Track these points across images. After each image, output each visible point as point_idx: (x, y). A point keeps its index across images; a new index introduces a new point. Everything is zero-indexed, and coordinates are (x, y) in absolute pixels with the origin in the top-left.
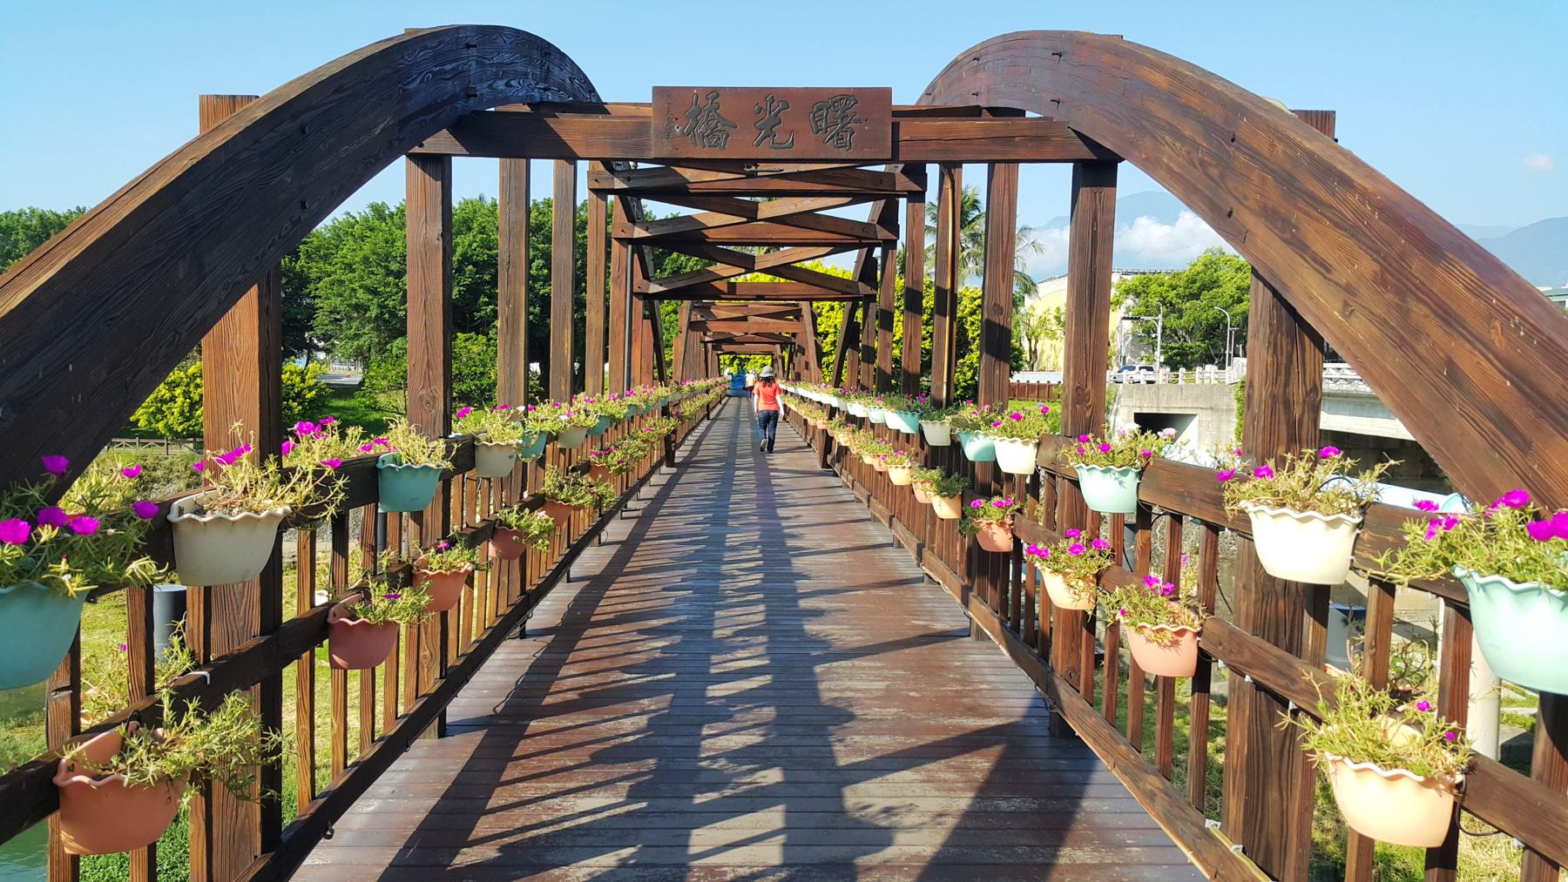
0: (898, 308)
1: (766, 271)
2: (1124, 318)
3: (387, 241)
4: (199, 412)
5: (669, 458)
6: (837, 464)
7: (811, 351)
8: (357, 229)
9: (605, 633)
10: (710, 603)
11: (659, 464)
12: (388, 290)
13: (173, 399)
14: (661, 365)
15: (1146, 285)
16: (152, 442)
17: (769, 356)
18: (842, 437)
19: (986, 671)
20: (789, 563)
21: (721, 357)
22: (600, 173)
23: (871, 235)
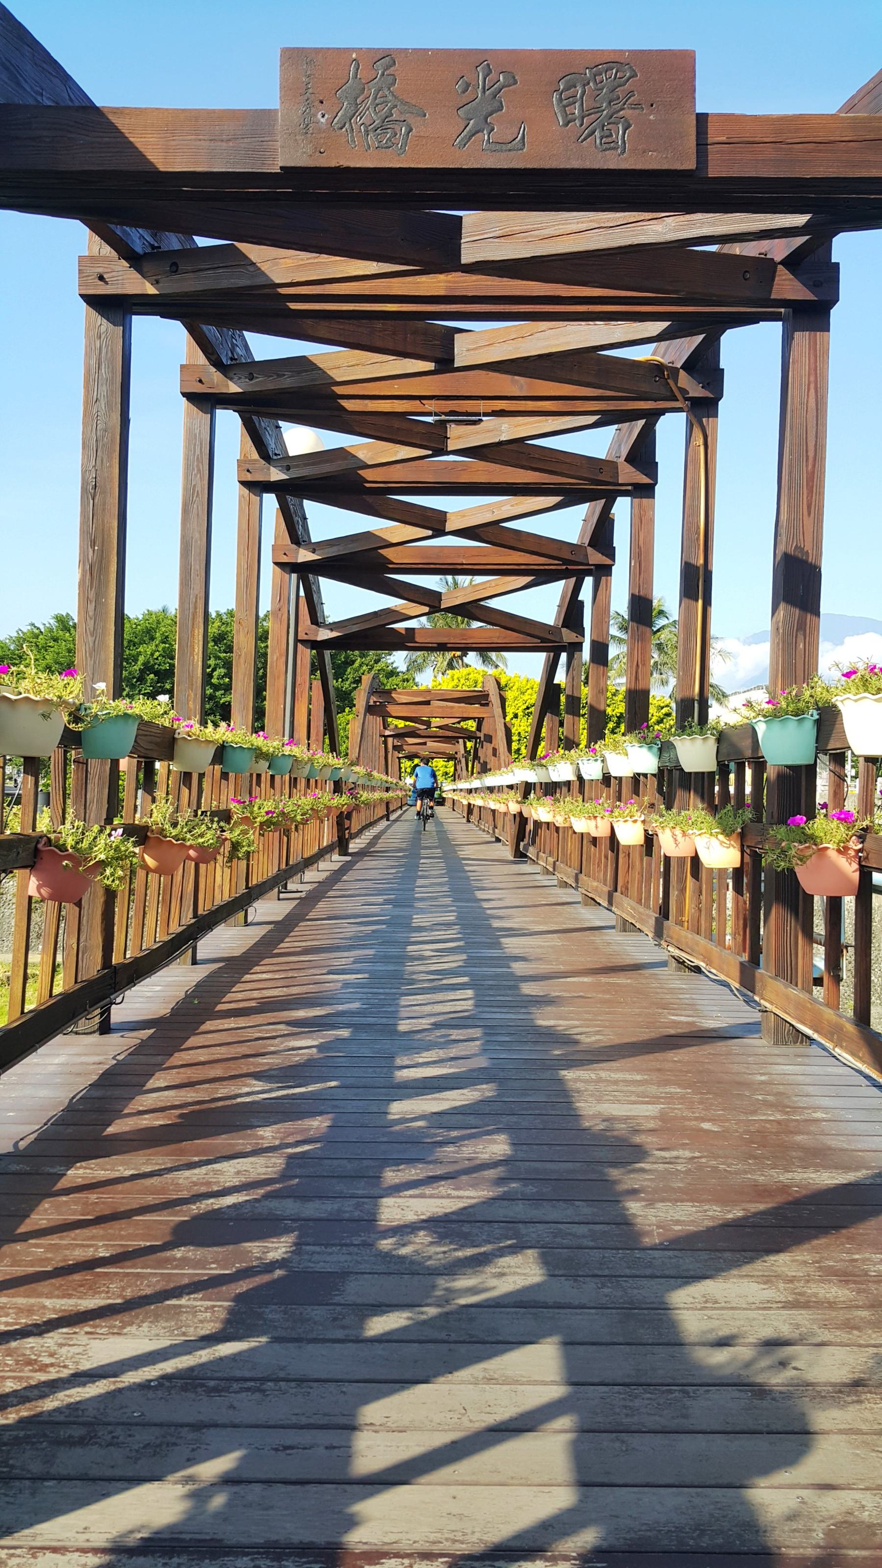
0: (583, 715)
5: (341, 845)
7: (501, 735)
8: (41, 640)
9: (226, 1026)
10: (381, 991)
19: (810, 1090)
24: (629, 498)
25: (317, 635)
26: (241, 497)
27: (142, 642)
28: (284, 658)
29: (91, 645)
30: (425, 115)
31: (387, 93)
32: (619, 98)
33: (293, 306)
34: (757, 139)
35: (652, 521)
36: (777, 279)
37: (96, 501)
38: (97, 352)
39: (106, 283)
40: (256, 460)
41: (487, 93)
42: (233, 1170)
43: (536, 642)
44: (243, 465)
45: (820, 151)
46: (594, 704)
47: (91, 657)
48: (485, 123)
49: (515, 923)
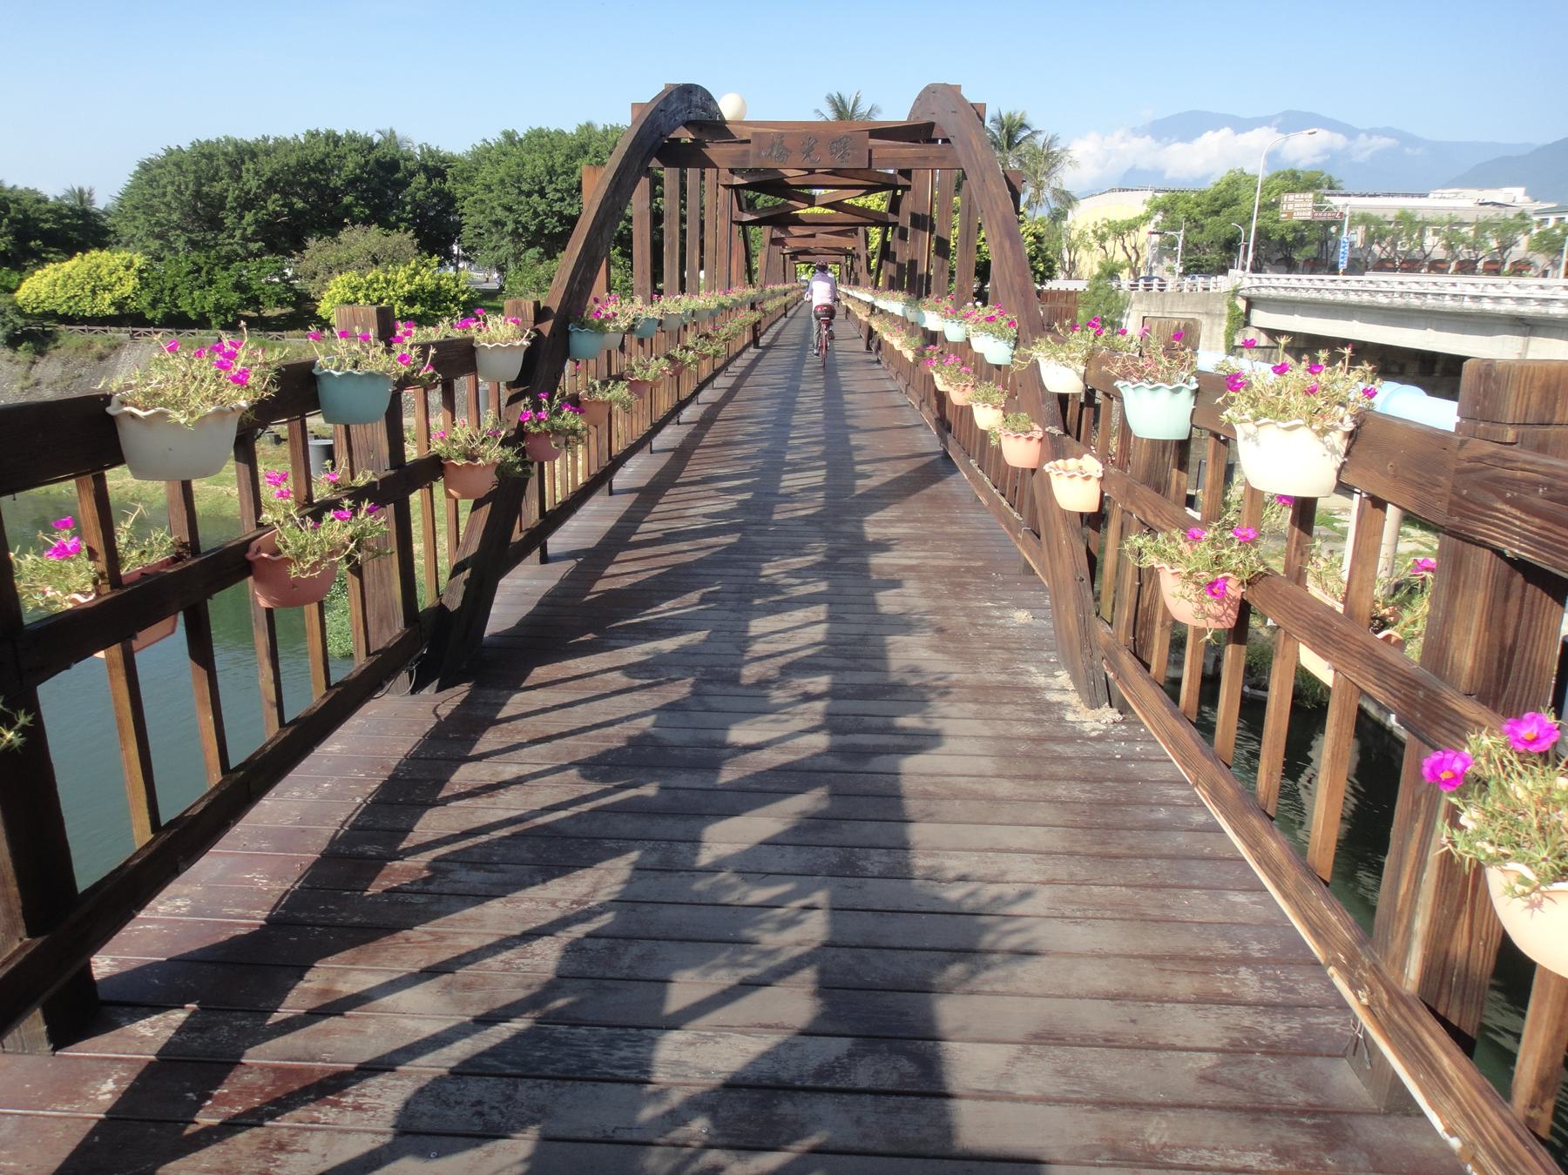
1: (825, 206)
5: (755, 341)
14: (750, 272)
15: (1173, 203)
27: (578, 156)
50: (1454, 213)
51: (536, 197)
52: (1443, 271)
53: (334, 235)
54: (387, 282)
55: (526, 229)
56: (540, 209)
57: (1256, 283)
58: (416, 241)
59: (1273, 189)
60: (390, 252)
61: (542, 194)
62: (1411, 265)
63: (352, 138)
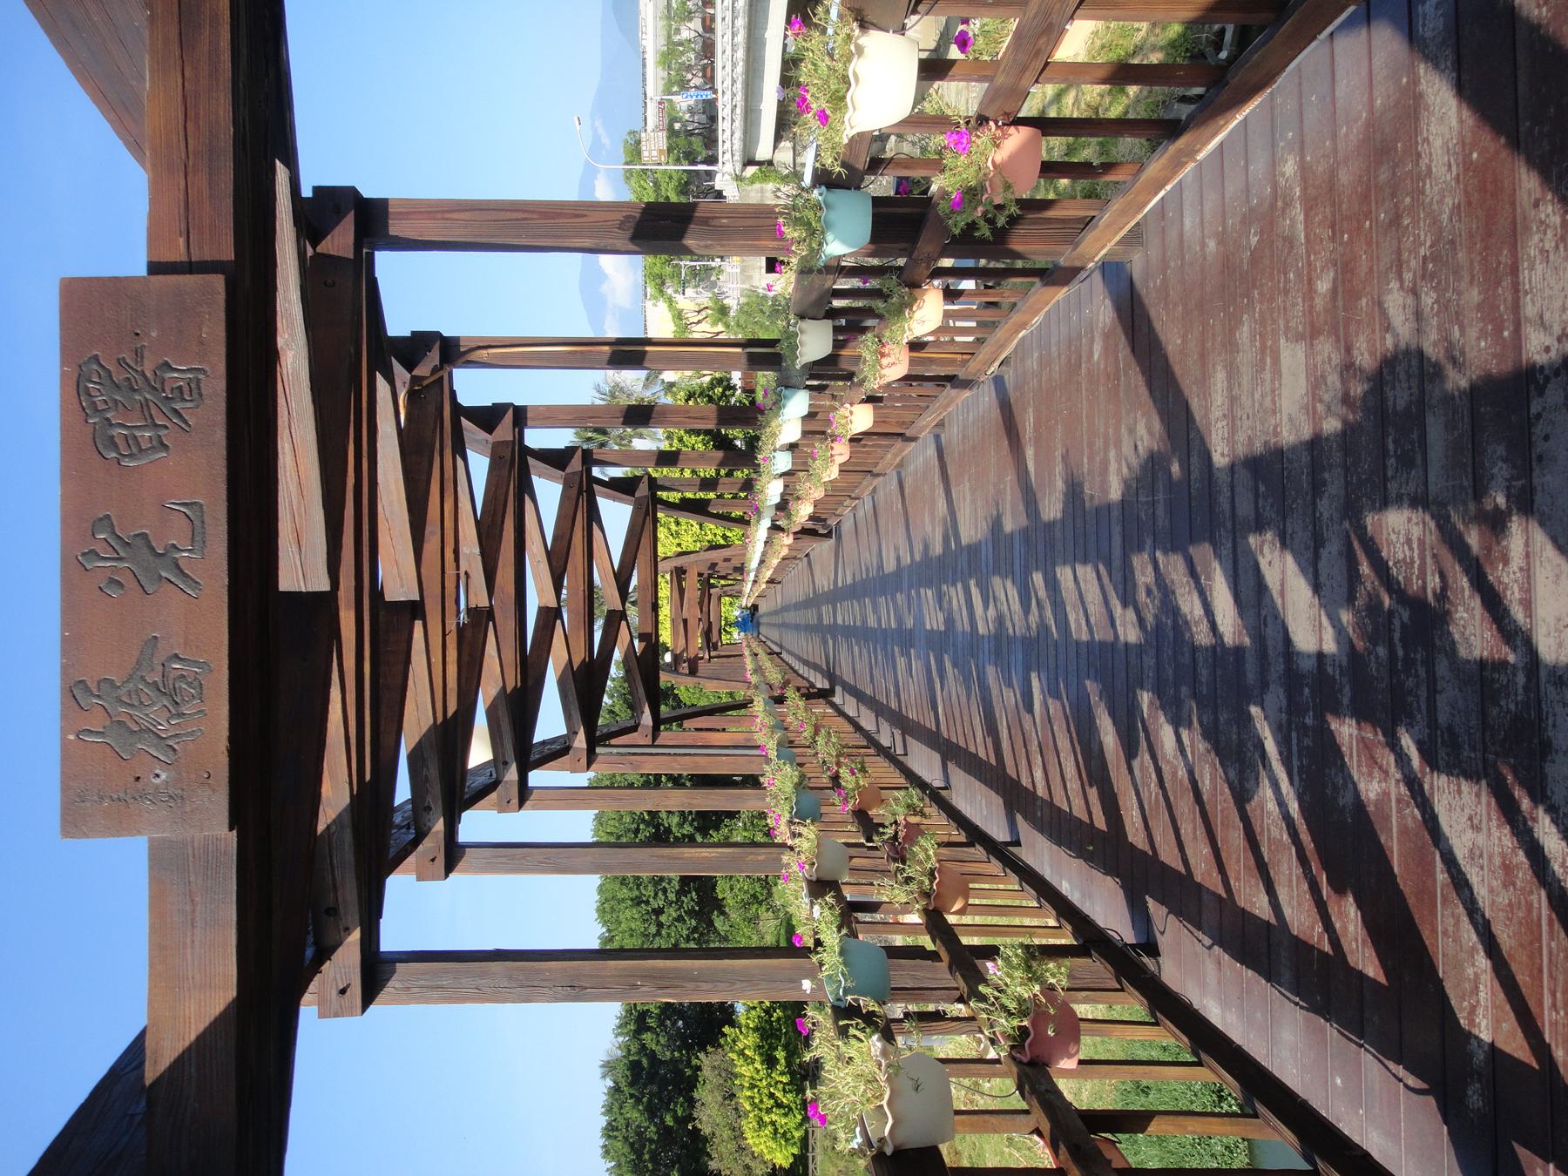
2: (684, 294)
3: (632, 936)
4: (784, 1100)
5: (825, 695)
6: (829, 522)
11: (833, 705)
12: (673, 934)
13: (773, 1123)
16: (811, 1141)
17: (723, 600)
18: (803, 512)
20: (1050, 525)
21: (724, 642)
22: (500, 798)
23: (577, 479)
24: (526, 430)
25: (647, 726)
26: (534, 808)
28: (678, 758)
29: (745, 984)
30: (155, 638)
31: (125, 690)
32: (128, 379)
33: (368, 777)
34: (182, 197)
35: (549, 408)
36: (332, 253)
37: (588, 985)
38: (425, 990)
39: (348, 985)
40: (498, 795)
41: (122, 554)
42: (1470, 834)
43: (649, 520)
44: (503, 807)
45: (197, 114)
46: (718, 462)
47: (758, 984)
48: (166, 556)
49: (934, 530)
50: (659, 15)
51: (663, 918)
52: (713, 18)
53: (705, 1140)
54: (752, 1087)
55: (695, 930)
56: (674, 915)
57: (728, 156)
58: (710, 1049)
59: (640, 186)
60: (722, 1082)
61: (659, 912)
62: (708, 49)
63: (609, 1110)
